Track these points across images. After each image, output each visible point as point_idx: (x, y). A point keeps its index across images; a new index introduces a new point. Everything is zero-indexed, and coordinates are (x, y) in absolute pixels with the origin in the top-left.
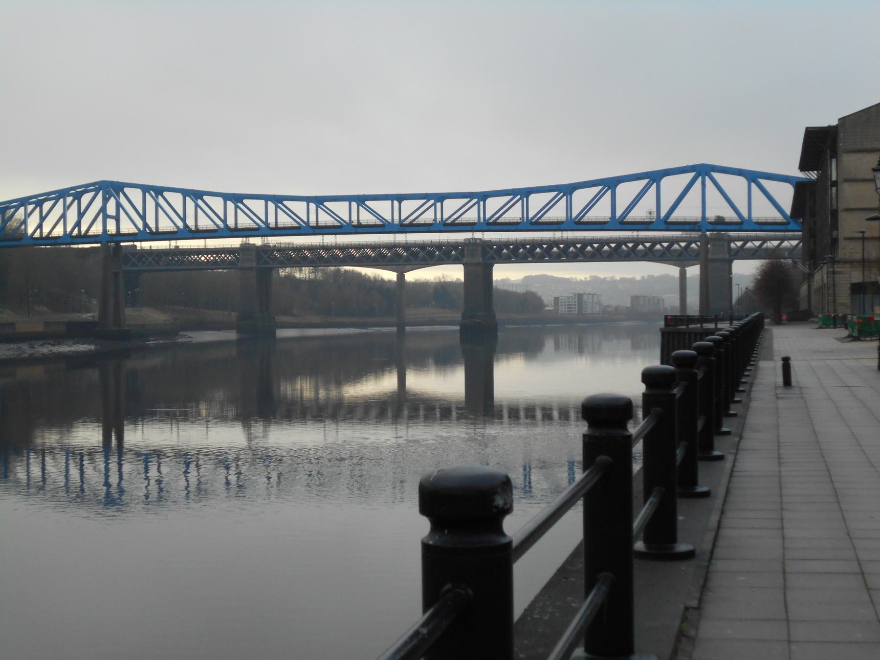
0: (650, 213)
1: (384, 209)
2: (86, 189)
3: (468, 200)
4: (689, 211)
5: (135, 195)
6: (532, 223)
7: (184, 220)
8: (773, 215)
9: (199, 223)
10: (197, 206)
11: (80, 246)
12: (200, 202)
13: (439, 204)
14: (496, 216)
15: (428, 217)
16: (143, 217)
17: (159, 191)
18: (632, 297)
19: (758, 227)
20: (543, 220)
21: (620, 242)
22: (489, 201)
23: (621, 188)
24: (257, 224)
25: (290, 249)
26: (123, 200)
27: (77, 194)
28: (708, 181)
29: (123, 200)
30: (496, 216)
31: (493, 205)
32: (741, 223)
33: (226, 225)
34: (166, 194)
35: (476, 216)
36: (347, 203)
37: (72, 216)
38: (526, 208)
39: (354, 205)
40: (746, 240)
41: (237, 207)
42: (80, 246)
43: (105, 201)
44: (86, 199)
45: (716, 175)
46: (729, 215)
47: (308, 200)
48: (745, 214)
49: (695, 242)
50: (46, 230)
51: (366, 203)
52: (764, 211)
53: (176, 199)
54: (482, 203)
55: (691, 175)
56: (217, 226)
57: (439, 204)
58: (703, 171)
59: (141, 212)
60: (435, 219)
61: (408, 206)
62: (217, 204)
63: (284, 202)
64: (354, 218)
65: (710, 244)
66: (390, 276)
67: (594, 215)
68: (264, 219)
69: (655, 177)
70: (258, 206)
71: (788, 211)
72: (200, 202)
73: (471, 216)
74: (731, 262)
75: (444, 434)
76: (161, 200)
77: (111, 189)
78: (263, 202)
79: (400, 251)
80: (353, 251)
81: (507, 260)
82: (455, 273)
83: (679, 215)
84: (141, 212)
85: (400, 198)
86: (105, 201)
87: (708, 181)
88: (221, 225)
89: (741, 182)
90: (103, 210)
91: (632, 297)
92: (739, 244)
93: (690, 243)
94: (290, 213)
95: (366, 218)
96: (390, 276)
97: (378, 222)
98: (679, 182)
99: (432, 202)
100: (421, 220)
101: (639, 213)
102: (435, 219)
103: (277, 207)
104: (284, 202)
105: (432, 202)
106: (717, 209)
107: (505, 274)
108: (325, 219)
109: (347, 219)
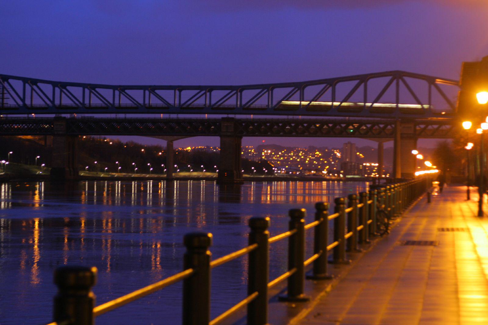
1: (169, 96)
3: (198, 91)
9: (33, 103)
10: (32, 89)
12: (35, 87)
13: (208, 94)
14: (249, 104)
15: (200, 102)
20: (252, 106)
22: (214, 93)
28: (401, 83)
30: (249, 104)
32: (137, 108)
33: (25, 104)
34: (10, 81)
35: (235, 103)
36: (81, 89)
39: (117, 92)
40: (361, 124)
41: (61, 91)
45: (406, 78)
47: (114, 88)
49: (390, 125)
51: (126, 91)
54: (239, 94)
55: (389, 78)
56: (48, 105)
57: (208, 94)
59: (22, 97)
60: (205, 105)
61: (186, 95)
62: (48, 89)
63: (97, 89)
64: (87, 102)
68: (81, 101)
70: (77, 92)
72: (35, 87)
73: (232, 102)
74: (241, 138)
78: (81, 89)
80: (138, 125)
84: (22, 97)
85: (181, 88)
87: (401, 83)
88: (20, 103)
92: (423, 126)
93: (373, 126)
97: (164, 106)
99: (204, 92)
102: (205, 105)
103: (90, 92)
104: (97, 89)
105: (204, 92)
108: (125, 101)
109: (111, 102)
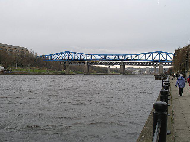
2: (64, 53)
4: (150, 58)
5: (72, 54)
7: (73, 57)
8: (170, 60)
11: (99, 66)
16: (73, 57)
17: (75, 53)
21: (145, 63)
26: (69, 54)
27: (63, 53)
29: (69, 54)
31: (120, 57)
37: (56, 57)
38: (132, 57)
39: (80, 55)
42: (99, 66)
43: (67, 54)
44: (64, 54)
46: (163, 59)
50: (52, 59)
52: (169, 59)
53: (78, 55)
55: (150, 54)
61: (114, 57)
62: (84, 55)
65: (163, 62)
66: (108, 67)
67: (142, 59)
69: (152, 53)
71: (173, 59)
75: (162, 102)
76: (75, 54)
77: (68, 53)
82: (119, 67)
83: (155, 59)
85: (112, 55)
86: (67, 54)
90: (67, 55)
94: (95, 57)
95: (107, 58)
96: (108, 67)
100: (122, 59)
101: (149, 59)
106: (161, 58)
107: (126, 67)
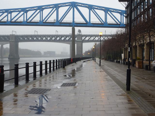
0: (55, 20)
6: (44, 23)
18: (61, 52)
19: (93, 25)
23: (60, 9)
24: (116, 22)
25: (24, 36)
38: (41, 16)
48: (88, 20)
57: (25, 14)
58: (74, 5)
60: (24, 20)
79: (6, 37)
81: (24, 41)
83: (66, 20)
89: (87, 10)
91: (61, 52)
94: (114, 18)
98: (65, 9)
100: (18, 21)
102: (40, 21)
105: (55, 9)
